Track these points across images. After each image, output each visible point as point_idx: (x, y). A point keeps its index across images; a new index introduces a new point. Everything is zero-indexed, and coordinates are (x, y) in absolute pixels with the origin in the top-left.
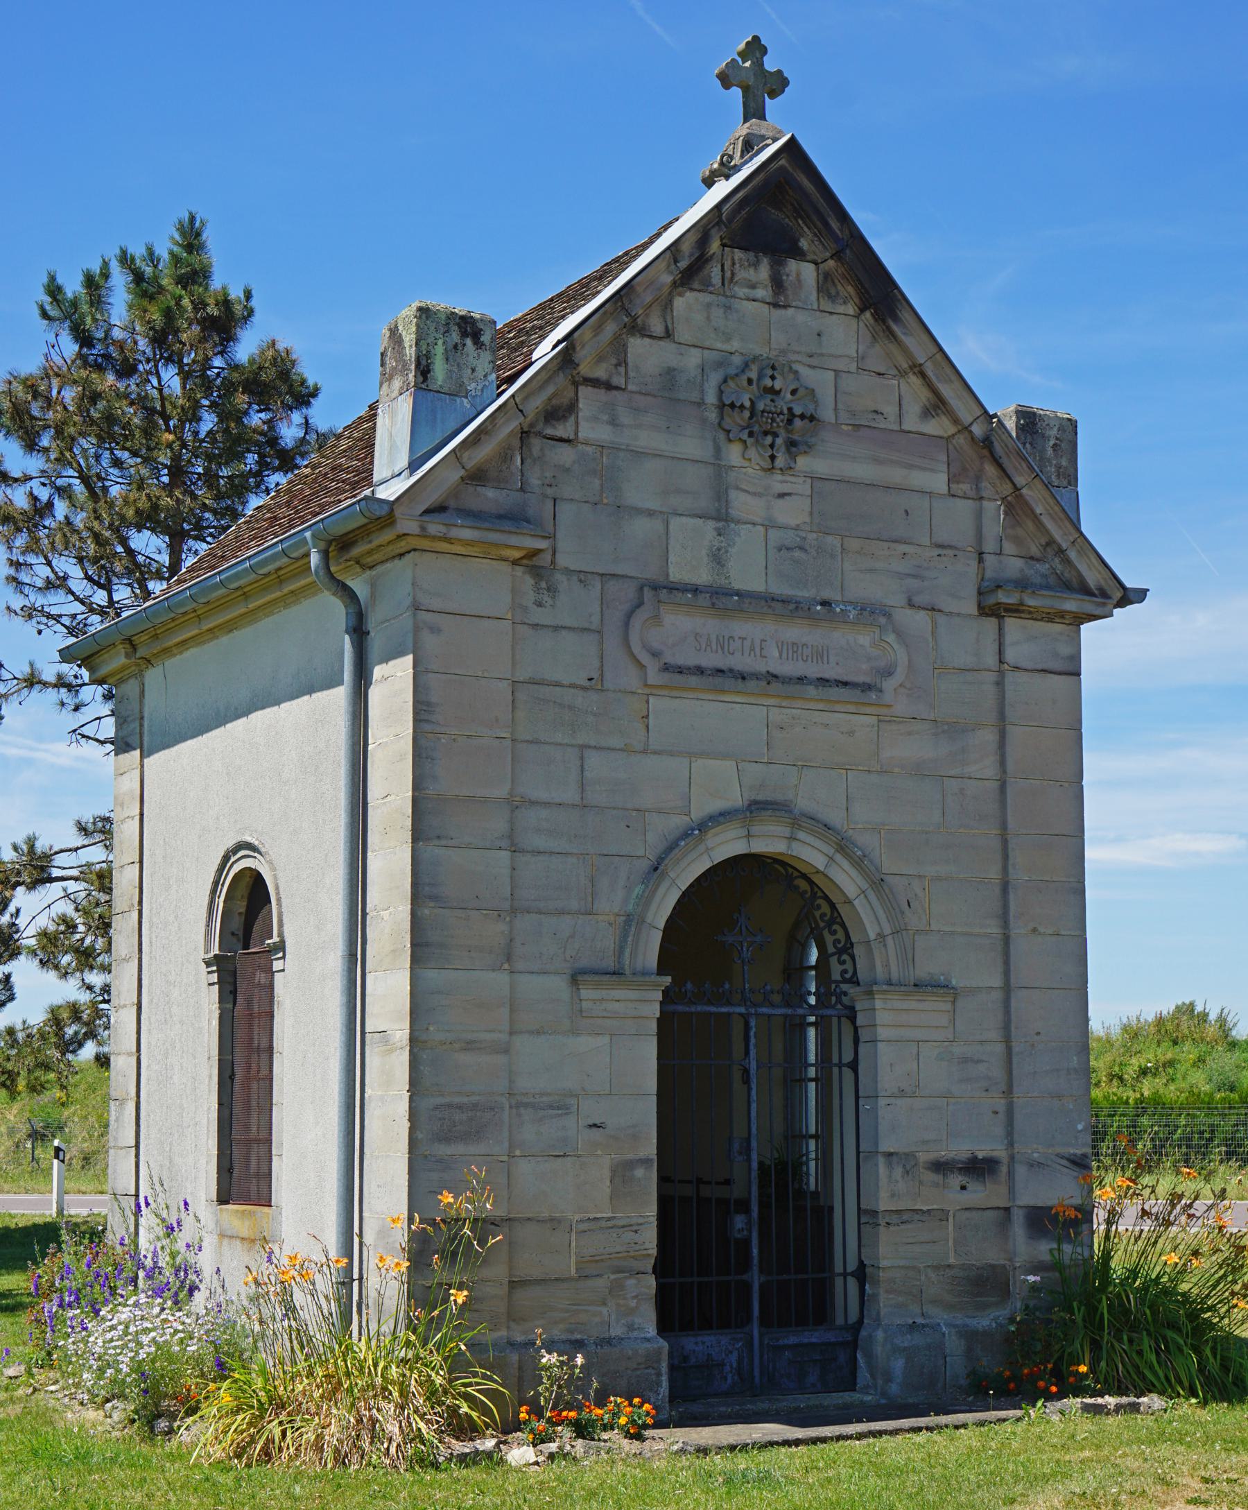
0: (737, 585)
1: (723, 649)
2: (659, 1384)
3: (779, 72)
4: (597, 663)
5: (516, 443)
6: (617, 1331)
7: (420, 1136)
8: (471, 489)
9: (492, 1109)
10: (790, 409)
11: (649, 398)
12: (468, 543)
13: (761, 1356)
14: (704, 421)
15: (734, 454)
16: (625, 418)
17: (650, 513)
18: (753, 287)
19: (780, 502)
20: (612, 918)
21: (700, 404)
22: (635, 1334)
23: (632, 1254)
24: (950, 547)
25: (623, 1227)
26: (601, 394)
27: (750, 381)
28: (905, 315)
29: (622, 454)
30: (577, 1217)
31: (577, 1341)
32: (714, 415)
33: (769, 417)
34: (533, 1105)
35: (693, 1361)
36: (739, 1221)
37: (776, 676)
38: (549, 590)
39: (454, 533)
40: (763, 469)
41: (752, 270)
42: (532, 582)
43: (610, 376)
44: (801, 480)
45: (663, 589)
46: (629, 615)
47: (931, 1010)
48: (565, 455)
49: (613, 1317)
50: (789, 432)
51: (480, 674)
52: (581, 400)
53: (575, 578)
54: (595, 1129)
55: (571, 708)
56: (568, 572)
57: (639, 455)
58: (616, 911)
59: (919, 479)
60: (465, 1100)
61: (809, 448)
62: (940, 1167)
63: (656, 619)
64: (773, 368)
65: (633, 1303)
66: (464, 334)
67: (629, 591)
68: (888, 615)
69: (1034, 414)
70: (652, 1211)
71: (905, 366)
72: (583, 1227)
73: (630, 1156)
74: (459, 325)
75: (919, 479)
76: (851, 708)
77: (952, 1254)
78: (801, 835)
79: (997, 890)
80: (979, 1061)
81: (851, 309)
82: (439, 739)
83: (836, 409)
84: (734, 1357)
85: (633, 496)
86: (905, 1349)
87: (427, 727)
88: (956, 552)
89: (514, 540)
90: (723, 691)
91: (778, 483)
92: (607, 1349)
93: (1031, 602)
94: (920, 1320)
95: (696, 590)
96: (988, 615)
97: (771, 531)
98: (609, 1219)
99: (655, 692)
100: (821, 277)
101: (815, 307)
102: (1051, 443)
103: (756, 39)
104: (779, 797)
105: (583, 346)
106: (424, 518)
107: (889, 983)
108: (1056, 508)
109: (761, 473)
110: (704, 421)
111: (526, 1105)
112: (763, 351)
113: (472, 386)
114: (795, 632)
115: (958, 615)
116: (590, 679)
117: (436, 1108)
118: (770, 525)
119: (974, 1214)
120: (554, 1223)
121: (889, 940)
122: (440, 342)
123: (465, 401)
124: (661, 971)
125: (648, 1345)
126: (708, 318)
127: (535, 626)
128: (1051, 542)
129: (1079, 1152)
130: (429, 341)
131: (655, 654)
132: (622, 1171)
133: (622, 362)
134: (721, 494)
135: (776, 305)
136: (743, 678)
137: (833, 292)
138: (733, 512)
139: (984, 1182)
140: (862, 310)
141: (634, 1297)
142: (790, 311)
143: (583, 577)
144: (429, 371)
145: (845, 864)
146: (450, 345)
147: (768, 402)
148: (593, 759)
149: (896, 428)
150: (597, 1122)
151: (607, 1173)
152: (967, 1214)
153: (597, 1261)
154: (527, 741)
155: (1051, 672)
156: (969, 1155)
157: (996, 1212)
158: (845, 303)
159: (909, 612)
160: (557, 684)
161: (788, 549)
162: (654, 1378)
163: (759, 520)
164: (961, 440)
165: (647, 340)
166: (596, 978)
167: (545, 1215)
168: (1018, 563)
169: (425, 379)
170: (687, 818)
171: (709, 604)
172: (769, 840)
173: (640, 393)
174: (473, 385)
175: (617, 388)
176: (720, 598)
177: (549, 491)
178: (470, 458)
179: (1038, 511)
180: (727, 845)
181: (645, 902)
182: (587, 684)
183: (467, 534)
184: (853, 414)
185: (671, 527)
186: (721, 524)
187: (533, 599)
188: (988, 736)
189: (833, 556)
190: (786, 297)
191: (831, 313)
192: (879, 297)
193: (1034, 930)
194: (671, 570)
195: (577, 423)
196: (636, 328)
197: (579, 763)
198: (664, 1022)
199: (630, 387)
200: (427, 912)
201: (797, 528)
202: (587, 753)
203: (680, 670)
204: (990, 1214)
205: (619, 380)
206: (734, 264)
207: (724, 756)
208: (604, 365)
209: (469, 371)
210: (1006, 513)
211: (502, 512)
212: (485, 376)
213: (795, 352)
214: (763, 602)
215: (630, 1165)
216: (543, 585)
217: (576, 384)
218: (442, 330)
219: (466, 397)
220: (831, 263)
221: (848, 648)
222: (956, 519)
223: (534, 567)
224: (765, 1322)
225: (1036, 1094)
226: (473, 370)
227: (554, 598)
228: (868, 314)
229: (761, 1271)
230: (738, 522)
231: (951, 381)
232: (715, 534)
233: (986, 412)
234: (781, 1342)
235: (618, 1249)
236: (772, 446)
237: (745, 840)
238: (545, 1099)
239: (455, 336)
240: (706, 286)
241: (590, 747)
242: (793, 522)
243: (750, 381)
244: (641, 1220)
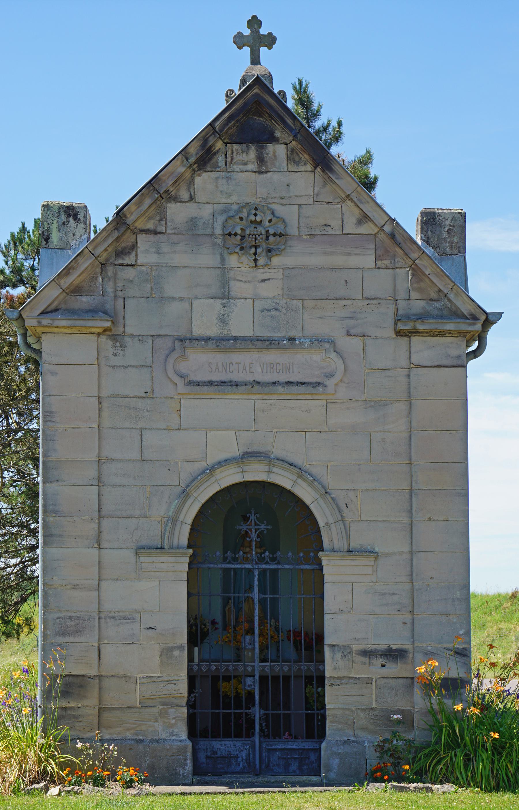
0: (235, 334)
1: (226, 370)
2: (185, 764)
3: (270, 34)
4: (149, 383)
5: (99, 270)
6: (163, 735)
7: (49, 632)
8: (73, 298)
9: (89, 619)
10: (267, 231)
11: (180, 236)
12: (68, 327)
14: (214, 244)
15: (233, 261)
16: (165, 248)
17: (181, 299)
18: (246, 164)
19: (263, 284)
20: (160, 519)
21: (212, 235)
22: (174, 737)
23: (172, 695)
24: (376, 298)
25: (168, 681)
26: (151, 238)
27: (241, 219)
28: (336, 168)
29: (163, 269)
30: (140, 675)
31: (140, 740)
32: (221, 240)
33: (256, 237)
34: (114, 617)
35: (219, 754)
36: (249, 681)
37: (258, 383)
38: (121, 347)
39: (57, 323)
40: (253, 267)
41: (244, 155)
42: (111, 343)
43: (156, 227)
44: (276, 271)
45: (188, 340)
46: (167, 356)
47: (360, 566)
48: (130, 273)
49: (161, 728)
50: (268, 244)
51: (80, 395)
52: (139, 242)
53: (136, 339)
54: (150, 630)
55: (134, 409)
56: (132, 336)
57: (174, 268)
58: (162, 515)
59: (354, 261)
60: (73, 614)
61: (280, 252)
62: (367, 653)
63: (183, 356)
64: (256, 209)
65: (173, 721)
66: (68, 216)
67: (168, 343)
68: (332, 342)
69: (434, 213)
70: (184, 674)
71: (344, 196)
72: (144, 680)
73: (171, 644)
74: (65, 211)
75: (354, 261)
76: (309, 397)
78: (275, 470)
79: (407, 496)
80: (393, 594)
81: (309, 167)
82: (57, 430)
83: (299, 227)
84: (244, 754)
85: (170, 291)
86: (339, 754)
87: (51, 424)
88: (380, 301)
89: (90, 324)
90: (227, 394)
91: (261, 274)
92: (155, 744)
93: (420, 327)
94: (352, 739)
95: (208, 339)
96: (402, 336)
97: (256, 302)
98: (159, 677)
99: (185, 396)
100: (289, 153)
101: (286, 170)
102: (446, 229)
103: (254, 17)
104: (261, 449)
105: (132, 214)
106: (40, 317)
107: (333, 550)
108: (438, 270)
109: (251, 269)
110: (214, 244)
111: (110, 617)
112: (251, 200)
113: (73, 243)
114: (272, 356)
115: (381, 337)
116: (146, 393)
117: (57, 619)
118: (255, 298)
119: (390, 680)
120: (127, 678)
121: (333, 527)
122: (55, 222)
123: (69, 251)
124: (189, 546)
125: (179, 744)
126: (217, 186)
127: (113, 367)
129: (460, 647)
130: (49, 222)
131: (182, 376)
132: (166, 653)
133: (163, 217)
134: (225, 284)
135: (260, 173)
136: (237, 385)
137: (297, 159)
138: (232, 293)
139: (397, 663)
140: (315, 168)
141: (174, 718)
142: (269, 174)
143: (141, 338)
144: (49, 238)
145: (304, 485)
146: (61, 223)
147: (252, 229)
148: (147, 435)
149: (339, 233)
150: (152, 626)
151: (157, 653)
152: (385, 680)
153: (152, 699)
154: (110, 428)
155: (444, 366)
156: (386, 647)
157: (405, 680)
158: (305, 164)
159: (348, 339)
160: (127, 397)
161: (267, 310)
162: (182, 761)
163: (249, 296)
164: (381, 235)
165: (178, 204)
166: (148, 551)
167: (122, 674)
168: (423, 303)
170: (205, 464)
171: (215, 346)
172: (256, 473)
173: (175, 234)
174: (74, 242)
175: (160, 233)
176: (223, 342)
177: (120, 294)
178: (65, 283)
180: (230, 477)
181: (179, 510)
182: (144, 395)
183: (64, 323)
184: (310, 228)
185: (194, 306)
186: (225, 301)
187: (112, 353)
188: (403, 407)
189: (297, 312)
190: (267, 167)
191: (296, 172)
193: (430, 518)
194: (194, 330)
195: (137, 255)
196: (170, 197)
197: (140, 438)
199: (168, 231)
200: (51, 519)
201: (274, 298)
202: (144, 432)
203: (198, 384)
204: (400, 681)
205: (162, 229)
206: (233, 153)
207: (227, 429)
208: (152, 221)
209: (72, 235)
210: (413, 275)
211: (91, 308)
212: (81, 237)
213: (272, 198)
214: (249, 342)
215: (171, 649)
216: (118, 344)
217: (136, 234)
218: (56, 215)
219: (70, 249)
220: (294, 143)
221: (304, 363)
222: (380, 282)
223: (113, 335)
225: (430, 613)
226: (74, 234)
227: (124, 351)
228: (318, 169)
229: (261, 707)
230: (236, 298)
231: (368, 202)
232: (221, 306)
233: (390, 218)
234: (273, 747)
235: (164, 693)
236: (255, 254)
237: (241, 474)
238: (121, 614)
239: (63, 218)
240: (215, 168)
241: (146, 429)
242: (271, 295)
243: (241, 219)
244: (178, 678)
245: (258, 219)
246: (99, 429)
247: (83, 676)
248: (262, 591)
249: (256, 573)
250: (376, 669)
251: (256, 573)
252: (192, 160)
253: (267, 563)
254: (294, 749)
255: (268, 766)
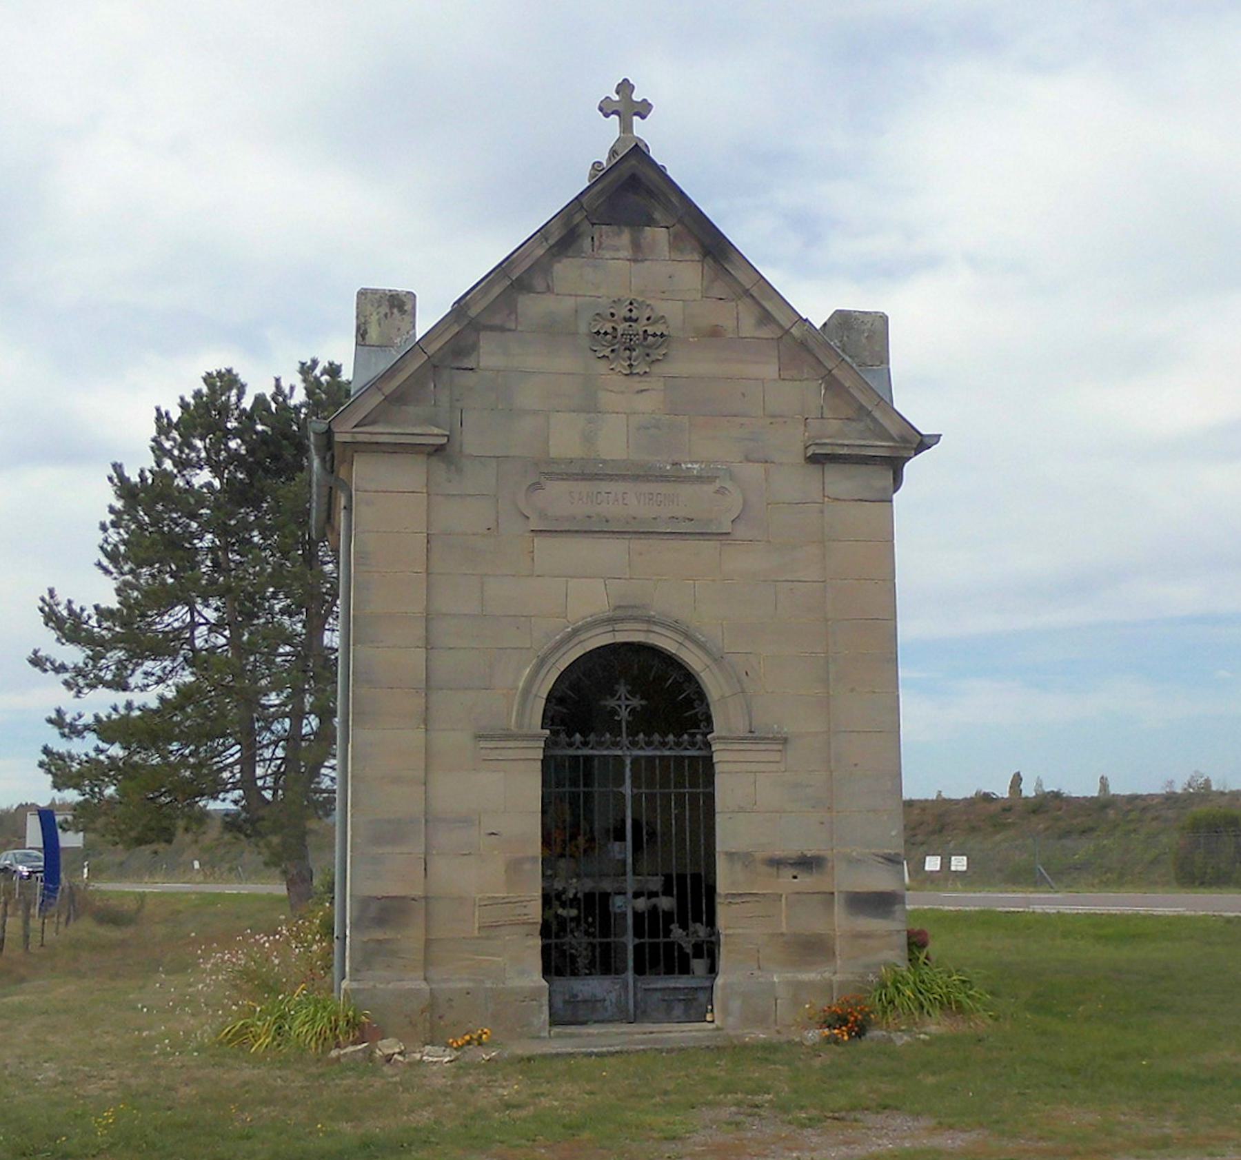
13: (635, 994)
18: (618, 250)
28: (735, 256)
33: (631, 340)
62: (776, 863)
66: (392, 306)
70: (538, 894)
77: (784, 924)
81: (696, 257)
128: (861, 407)
132: (514, 866)
135: (635, 261)
142: (647, 263)
146: (382, 315)
169: (364, 339)
175: (509, 330)
179: (847, 385)
192: (713, 247)
198: (545, 762)
199: (519, 328)
210: (826, 389)
221: (689, 501)
224: (639, 970)
239: (385, 309)
245: (634, 315)
246: (428, 574)
247: (403, 898)
248: (635, 784)
249: (628, 762)
250: (786, 882)
251: (628, 762)
252: (552, 242)
253: (642, 748)
254: (679, 989)
255: (644, 1012)
